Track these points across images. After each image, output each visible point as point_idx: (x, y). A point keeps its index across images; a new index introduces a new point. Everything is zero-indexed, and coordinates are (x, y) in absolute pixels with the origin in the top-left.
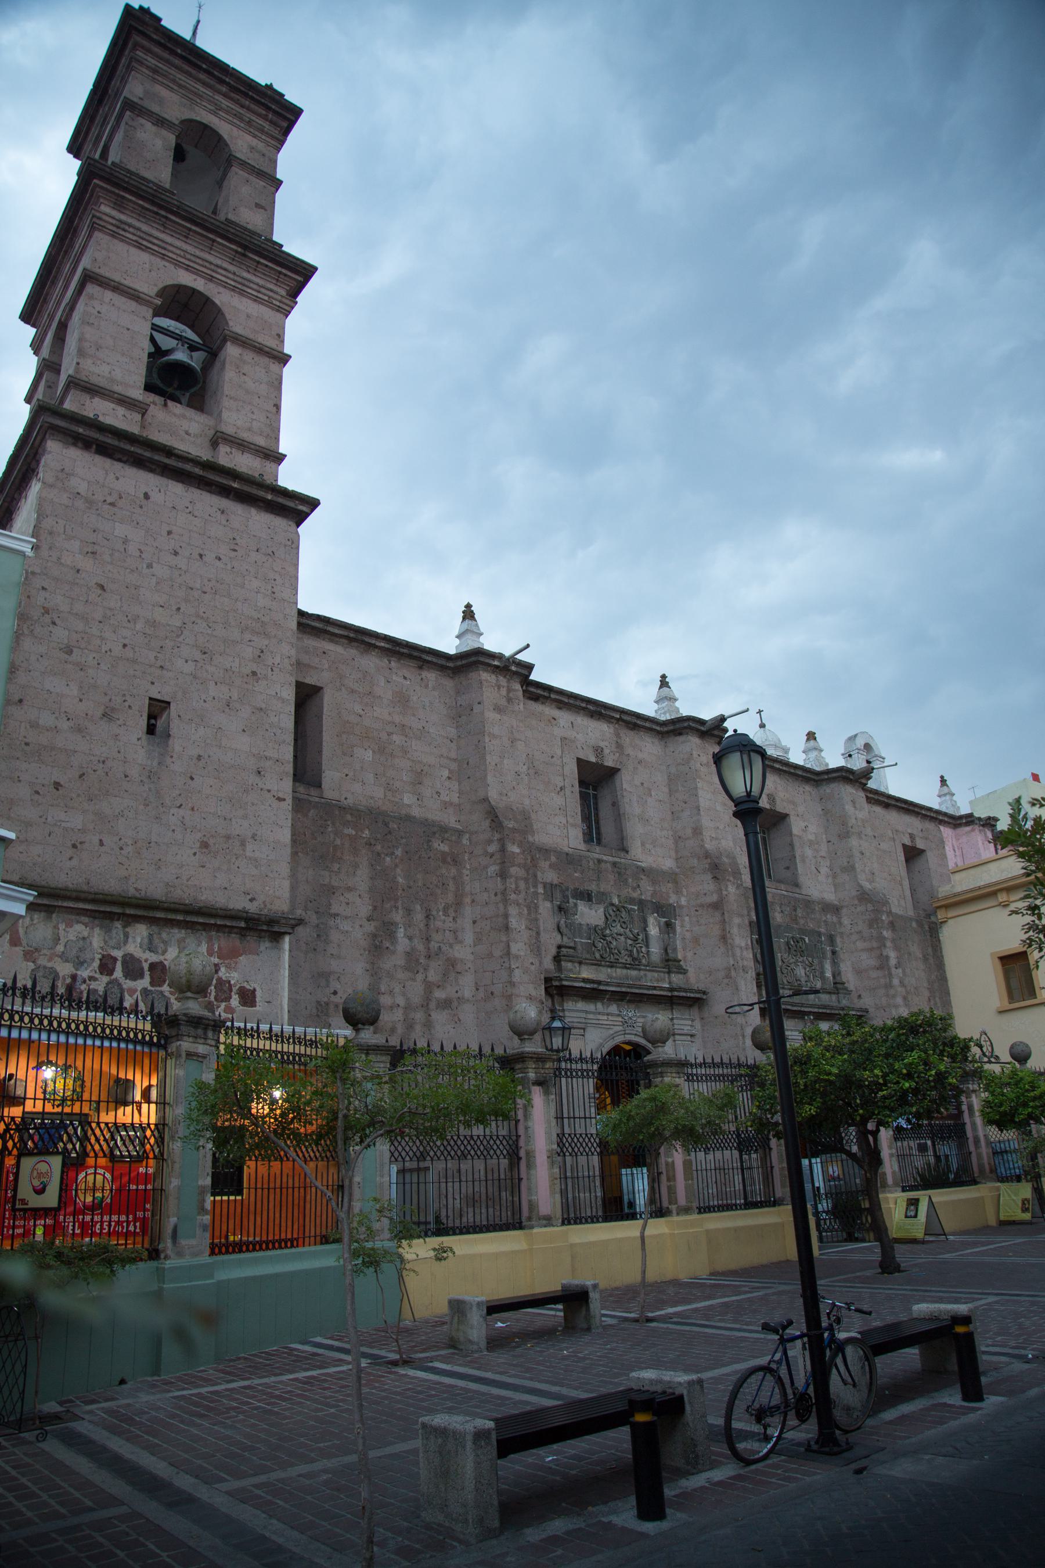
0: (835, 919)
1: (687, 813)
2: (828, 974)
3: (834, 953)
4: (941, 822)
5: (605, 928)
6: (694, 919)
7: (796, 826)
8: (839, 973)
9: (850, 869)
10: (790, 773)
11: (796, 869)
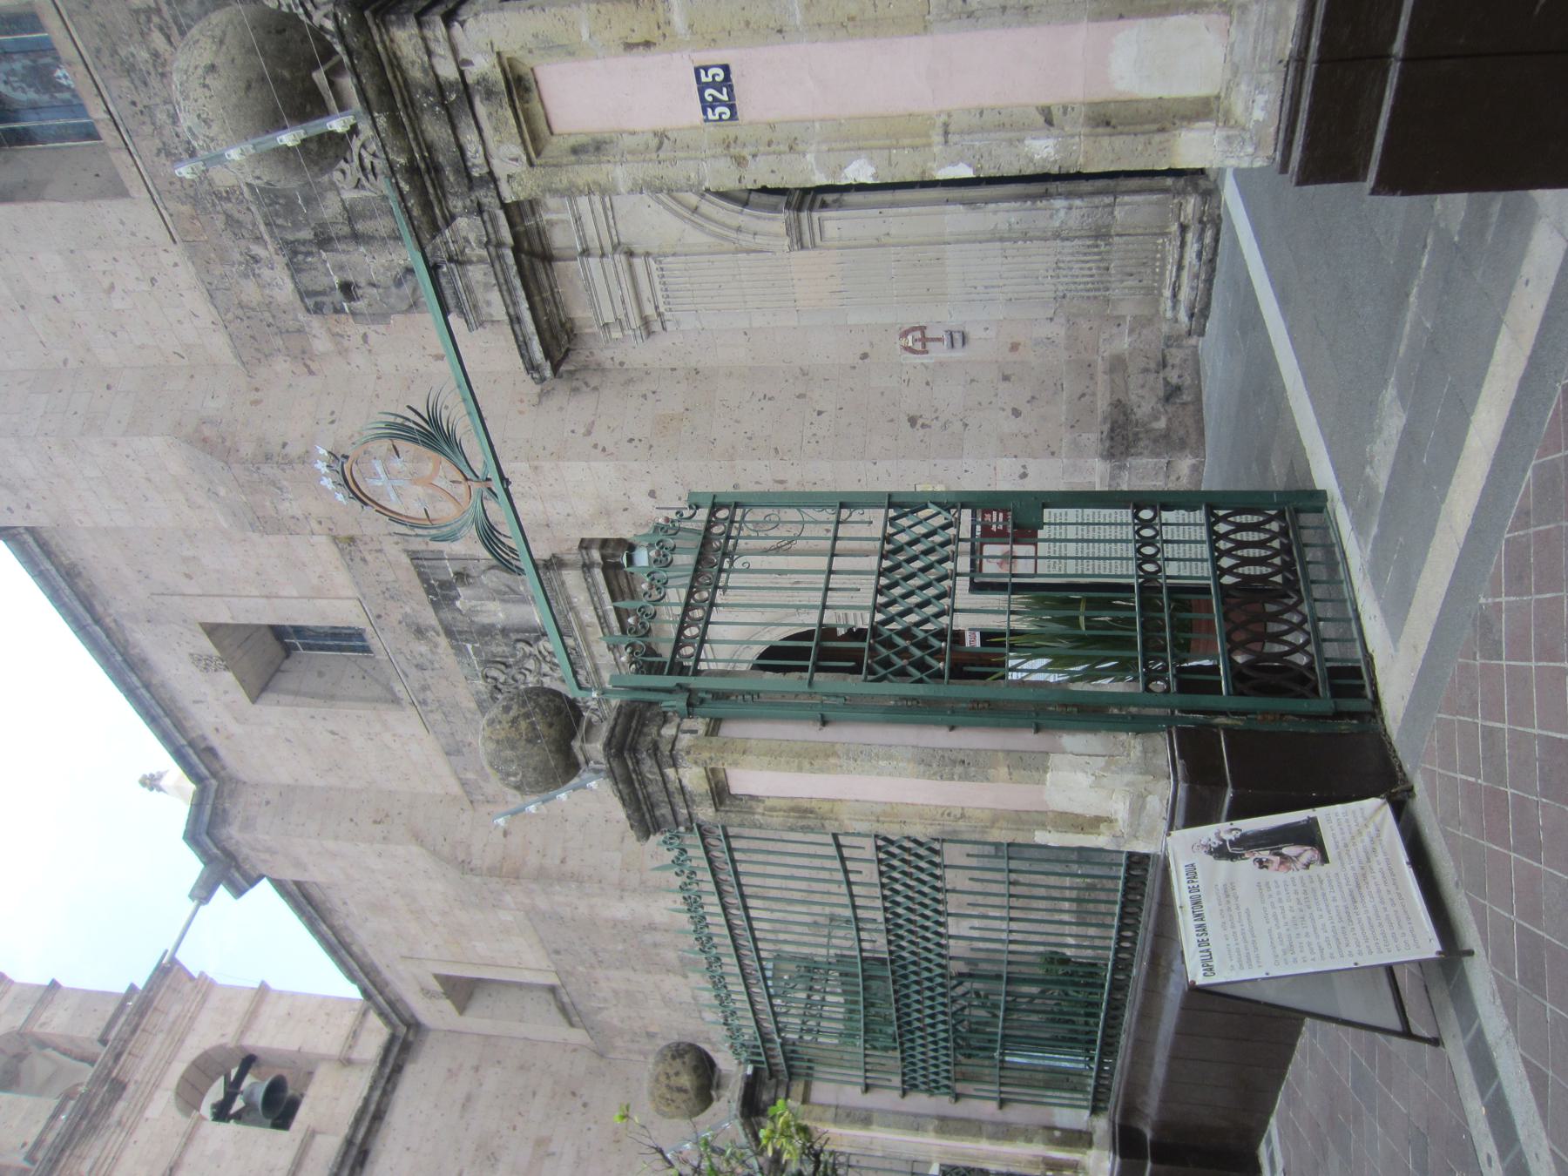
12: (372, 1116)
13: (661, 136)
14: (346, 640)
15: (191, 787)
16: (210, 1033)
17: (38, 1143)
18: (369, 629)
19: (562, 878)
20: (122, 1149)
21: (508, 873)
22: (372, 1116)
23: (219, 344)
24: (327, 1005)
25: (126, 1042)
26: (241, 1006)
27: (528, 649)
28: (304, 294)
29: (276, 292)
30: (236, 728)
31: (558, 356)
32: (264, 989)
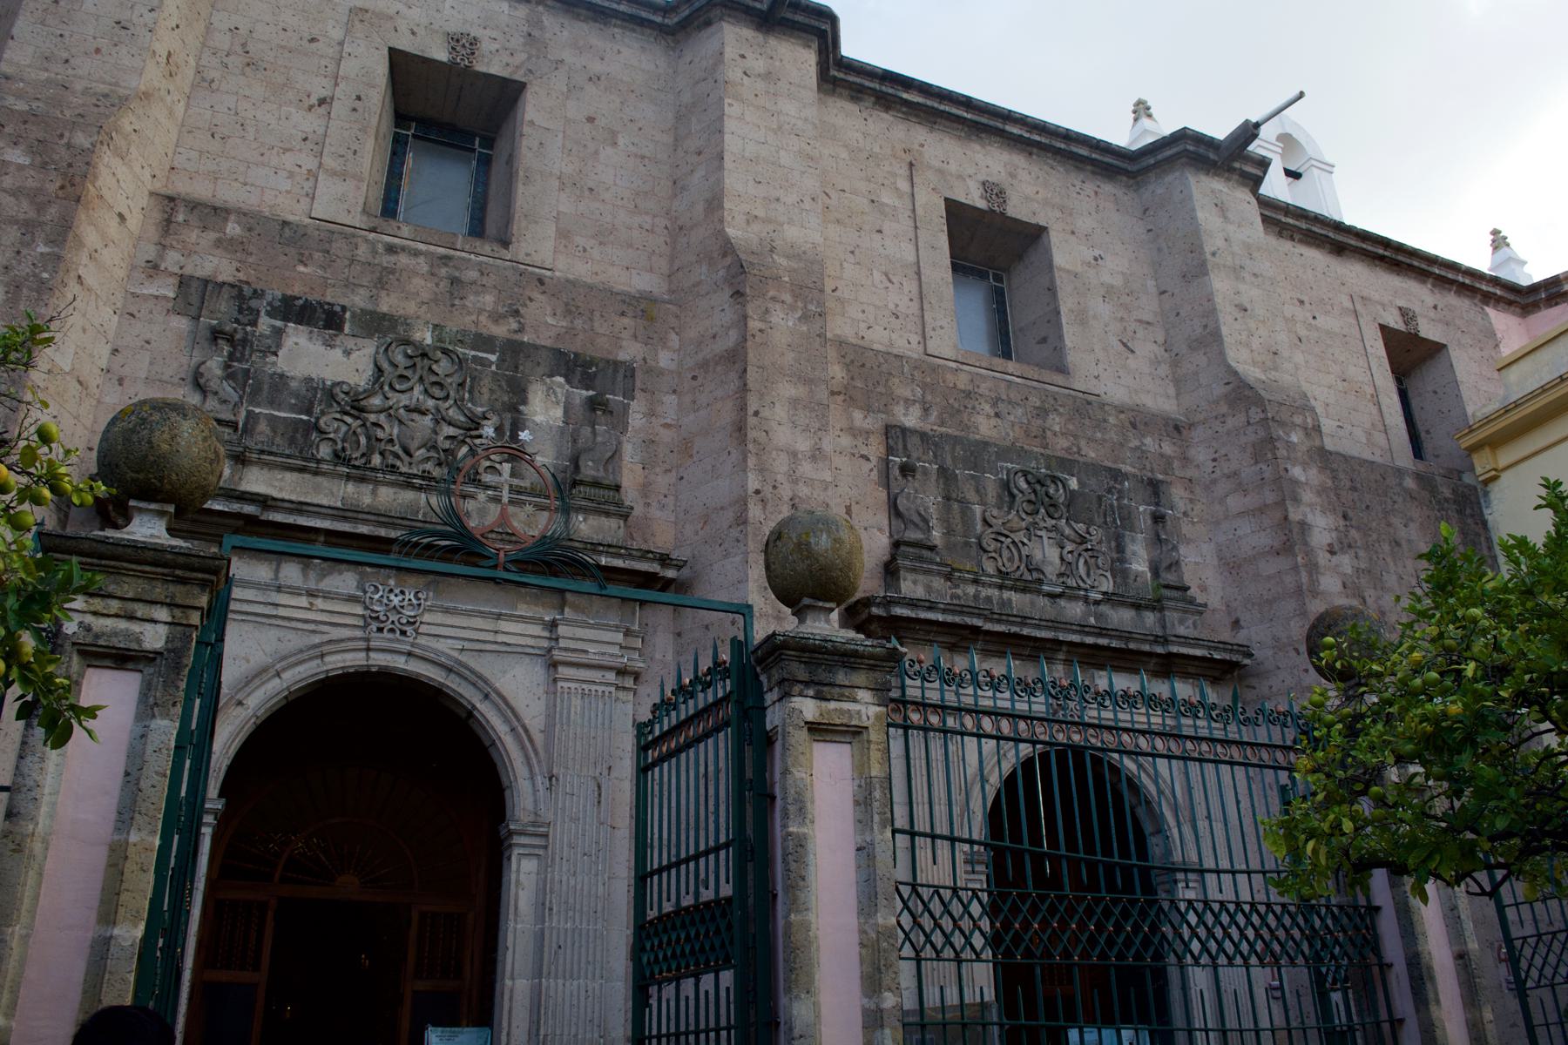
0: (1168, 449)
1: (700, 173)
2: (1140, 565)
3: (1158, 519)
4: (1487, 298)
5: (370, 393)
6: (687, 399)
7: (1065, 253)
8: (1175, 565)
9: (1211, 339)
10: (1057, 152)
11: (1061, 337)
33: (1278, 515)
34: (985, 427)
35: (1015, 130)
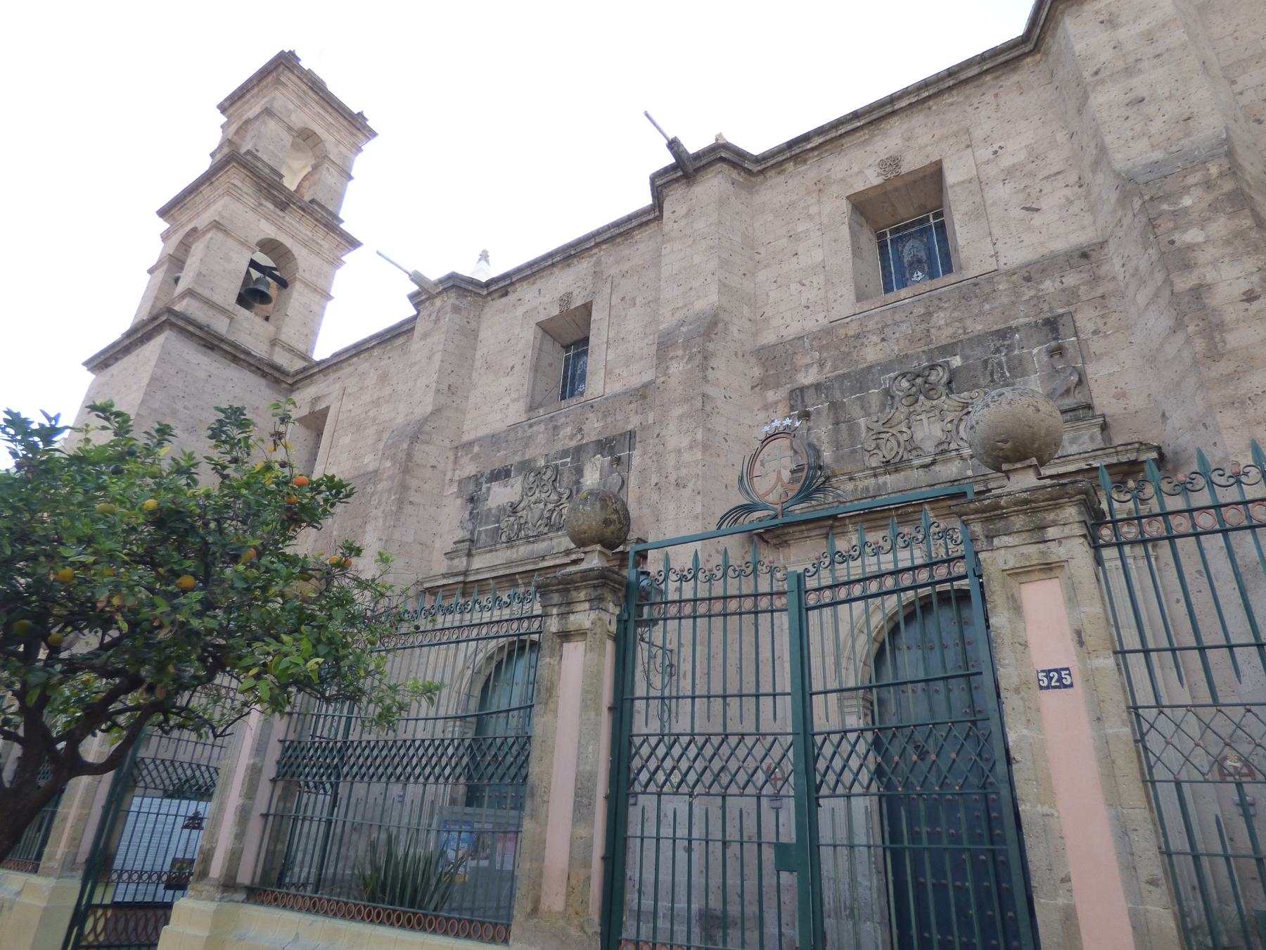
12: (237, 356)
13: (1025, 645)
14: (572, 382)
15: (484, 279)
16: (305, 260)
17: (256, 157)
18: (583, 399)
19: (400, 502)
20: (244, 204)
21: (407, 466)
22: (237, 356)
23: (769, 338)
24: (311, 335)
25: (311, 215)
26: (321, 283)
27: (565, 496)
28: (802, 389)
29: (803, 374)
30: (521, 310)
31: (766, 537)
32: (328, 297)
33: (1168, 292)
34: (872, 353)
35: (903, 103)
